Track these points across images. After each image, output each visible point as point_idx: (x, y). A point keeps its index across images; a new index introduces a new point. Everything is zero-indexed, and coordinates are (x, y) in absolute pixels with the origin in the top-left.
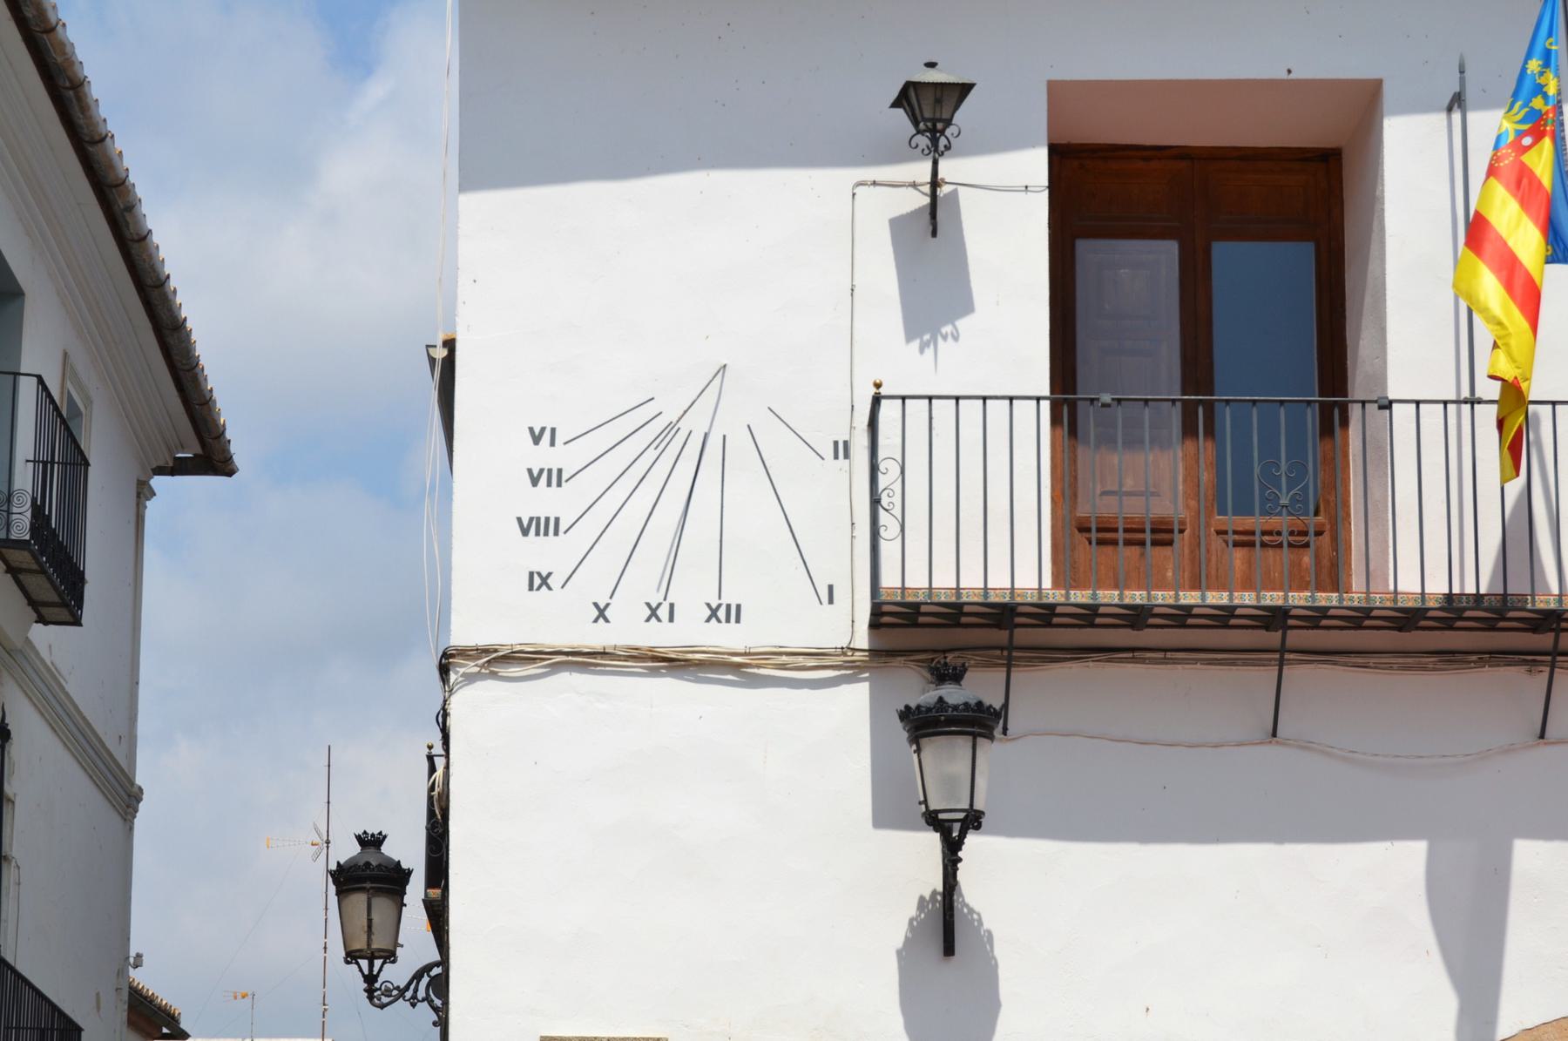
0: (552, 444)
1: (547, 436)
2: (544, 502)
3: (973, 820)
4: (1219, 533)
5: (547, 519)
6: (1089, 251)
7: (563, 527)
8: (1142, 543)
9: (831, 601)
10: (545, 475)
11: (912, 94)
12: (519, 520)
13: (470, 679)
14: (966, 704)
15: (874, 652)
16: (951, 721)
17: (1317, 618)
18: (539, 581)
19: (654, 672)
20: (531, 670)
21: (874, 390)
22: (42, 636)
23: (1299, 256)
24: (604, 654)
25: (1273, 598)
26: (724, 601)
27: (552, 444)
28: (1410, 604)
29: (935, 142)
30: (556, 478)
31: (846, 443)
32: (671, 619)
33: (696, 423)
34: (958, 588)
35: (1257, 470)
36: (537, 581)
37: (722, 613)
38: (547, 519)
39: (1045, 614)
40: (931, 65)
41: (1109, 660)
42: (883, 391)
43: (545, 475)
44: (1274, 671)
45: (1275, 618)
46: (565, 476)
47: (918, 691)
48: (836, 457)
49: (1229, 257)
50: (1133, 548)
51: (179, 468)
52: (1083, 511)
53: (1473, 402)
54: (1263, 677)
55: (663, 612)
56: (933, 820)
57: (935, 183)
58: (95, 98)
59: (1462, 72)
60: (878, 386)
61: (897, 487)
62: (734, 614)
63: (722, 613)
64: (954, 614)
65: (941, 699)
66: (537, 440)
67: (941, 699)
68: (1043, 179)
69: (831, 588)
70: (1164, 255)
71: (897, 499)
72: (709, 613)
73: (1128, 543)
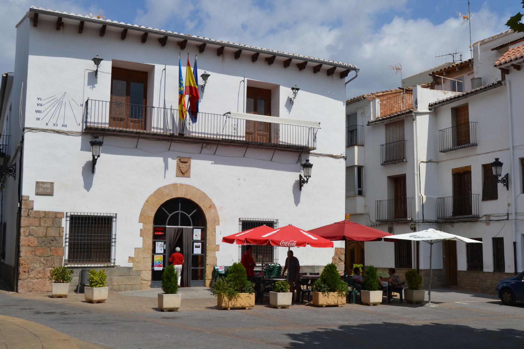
0: (41, 100)
1: (40, 99)
2: (39, 108)
5: (40, 111)
7: (42, 112)
9: (79, 125)
10: (39, 105)
11: (95, 59)
12: (36, 110)
14: (99, 142)
16: (97, 144)
17: (143, 133)
18: (38, 119)
20: (38, 131)
21: (88, 99)
23: (142, 85)
24: (47, 130)
25: (138, 131)
26: (64, 124)
27: (41, 100)
28: (155, 133)
29: (97, 66)
30: (41, 105)
31: (82, 105)
32: (57, 126)
34: (195, 136)
35: (137, 114)
36: (38, 119)
37: (64, 126)
38: (40, 111)
39: (109, 130)
40: (97, 56)
41: (153, 140)
42: (89, 99)
43: (39, 105)
44: (137, 139)
46: (42, 105)
48: (81, 106)
49: (133, 84)
52: (112, 116)
54: (273, 151)
55: (56, 125)
58: (495, 160)
60: (88, 98)
61: (232, 130)
62: (66, 126)
63: (64, 126)
65: (96, 141)
66: (38, 99)
67: (96, 141)
68: (111, 72)
69: (79, 124)
71: (90, 113)
72: (62, 125)
73: (117, 120)
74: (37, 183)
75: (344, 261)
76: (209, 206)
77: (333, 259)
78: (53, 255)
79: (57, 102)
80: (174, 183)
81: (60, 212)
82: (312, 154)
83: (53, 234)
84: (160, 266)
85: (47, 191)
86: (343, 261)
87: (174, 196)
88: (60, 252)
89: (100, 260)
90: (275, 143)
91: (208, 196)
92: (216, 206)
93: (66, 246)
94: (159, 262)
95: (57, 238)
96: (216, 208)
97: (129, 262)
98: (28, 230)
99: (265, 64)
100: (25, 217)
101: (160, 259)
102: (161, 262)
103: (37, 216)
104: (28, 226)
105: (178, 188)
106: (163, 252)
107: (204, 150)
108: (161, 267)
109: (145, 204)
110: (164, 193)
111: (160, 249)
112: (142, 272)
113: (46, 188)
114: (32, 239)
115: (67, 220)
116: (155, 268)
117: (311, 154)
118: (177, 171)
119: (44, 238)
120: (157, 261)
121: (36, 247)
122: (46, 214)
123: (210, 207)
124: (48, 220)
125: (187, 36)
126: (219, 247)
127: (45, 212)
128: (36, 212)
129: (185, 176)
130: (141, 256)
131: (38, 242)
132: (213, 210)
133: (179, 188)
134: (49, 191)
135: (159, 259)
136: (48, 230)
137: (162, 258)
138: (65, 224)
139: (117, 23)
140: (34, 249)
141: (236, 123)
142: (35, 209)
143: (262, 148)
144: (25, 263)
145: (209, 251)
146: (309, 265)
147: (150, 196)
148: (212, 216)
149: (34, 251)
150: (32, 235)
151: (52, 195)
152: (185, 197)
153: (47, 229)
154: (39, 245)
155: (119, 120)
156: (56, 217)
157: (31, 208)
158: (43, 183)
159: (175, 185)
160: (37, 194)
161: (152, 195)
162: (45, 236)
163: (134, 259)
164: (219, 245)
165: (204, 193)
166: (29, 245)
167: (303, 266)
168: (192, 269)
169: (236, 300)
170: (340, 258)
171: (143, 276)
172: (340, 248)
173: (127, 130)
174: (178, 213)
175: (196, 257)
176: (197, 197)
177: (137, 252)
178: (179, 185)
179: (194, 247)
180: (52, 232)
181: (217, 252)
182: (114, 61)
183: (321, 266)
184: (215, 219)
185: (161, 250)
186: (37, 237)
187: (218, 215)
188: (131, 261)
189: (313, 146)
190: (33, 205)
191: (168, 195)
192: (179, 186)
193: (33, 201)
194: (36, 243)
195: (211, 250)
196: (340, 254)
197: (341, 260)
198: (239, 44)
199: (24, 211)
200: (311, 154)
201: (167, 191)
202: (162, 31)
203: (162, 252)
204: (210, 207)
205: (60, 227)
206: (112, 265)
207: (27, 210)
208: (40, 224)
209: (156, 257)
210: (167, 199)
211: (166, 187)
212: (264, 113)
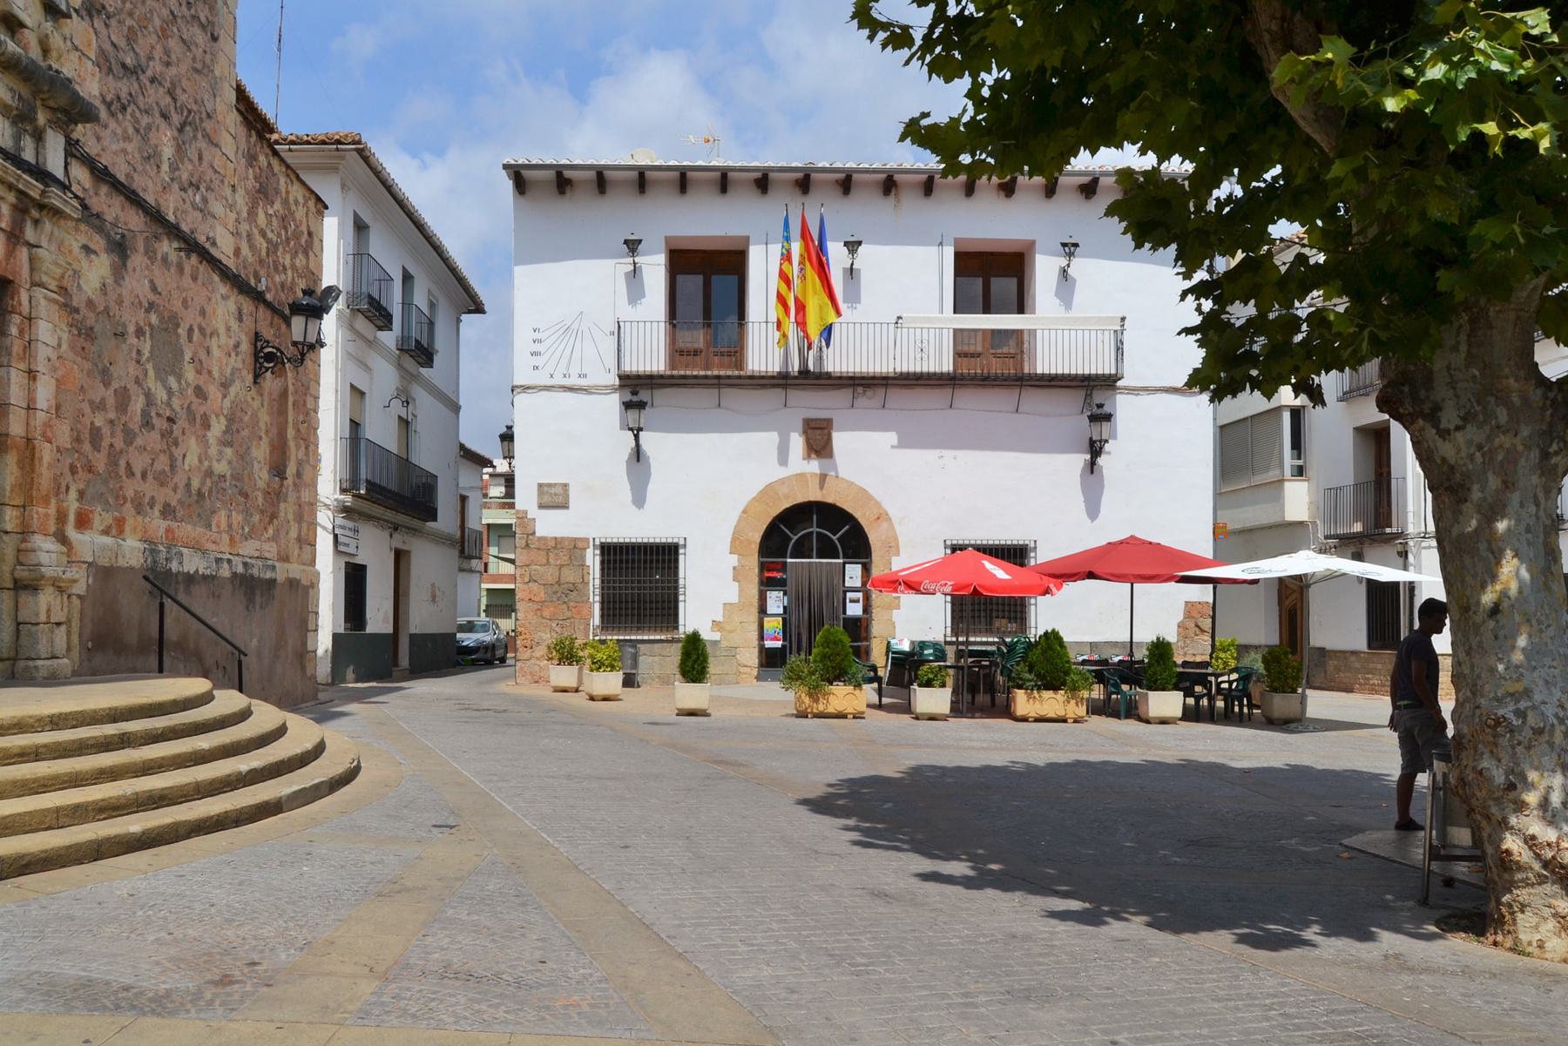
3: (640, 429)
6: (680, 278)
15: (620, 386)
17: (740, 377)
22: (423, 371)
30: (540, 341)
33: (575, 326)
39: (662, 377)
45: (718, 377)
47: (628, 397)
50: (147, 583)
51: (470, 312)
56: (631, 429)
57: (635, 263)
62: (585, 376)
64: (638, 377)
70: (699, 279)
74: (540, 486)
77: (1179, 627)
83: (571, 579)
84: (776, 639)
87: (800, 499)
88: (585, 612)
96: (890, 520)
109: (740, 517)
113: (556, 494)
119: (557, 586)
122: (558, 542)
132: (885, 525)
134: (560, 500)
135: (773, 625)
138: (593, 560)
142: (537, 534)
143: (994, 386)
150: (535, 581)
151: (567, 508)
156: (575, 547)
158: (550, 485)
160: (541, 506)
174: (812, 532)
180: (569, 576)
185: (779, 607)
191: (787, 497)
194: (542, 595)
197: (1203, 631)
199: (520, 539)
201: (784, 490)
203: (781, 611)
205: (583, 565)
209: (769, 622)
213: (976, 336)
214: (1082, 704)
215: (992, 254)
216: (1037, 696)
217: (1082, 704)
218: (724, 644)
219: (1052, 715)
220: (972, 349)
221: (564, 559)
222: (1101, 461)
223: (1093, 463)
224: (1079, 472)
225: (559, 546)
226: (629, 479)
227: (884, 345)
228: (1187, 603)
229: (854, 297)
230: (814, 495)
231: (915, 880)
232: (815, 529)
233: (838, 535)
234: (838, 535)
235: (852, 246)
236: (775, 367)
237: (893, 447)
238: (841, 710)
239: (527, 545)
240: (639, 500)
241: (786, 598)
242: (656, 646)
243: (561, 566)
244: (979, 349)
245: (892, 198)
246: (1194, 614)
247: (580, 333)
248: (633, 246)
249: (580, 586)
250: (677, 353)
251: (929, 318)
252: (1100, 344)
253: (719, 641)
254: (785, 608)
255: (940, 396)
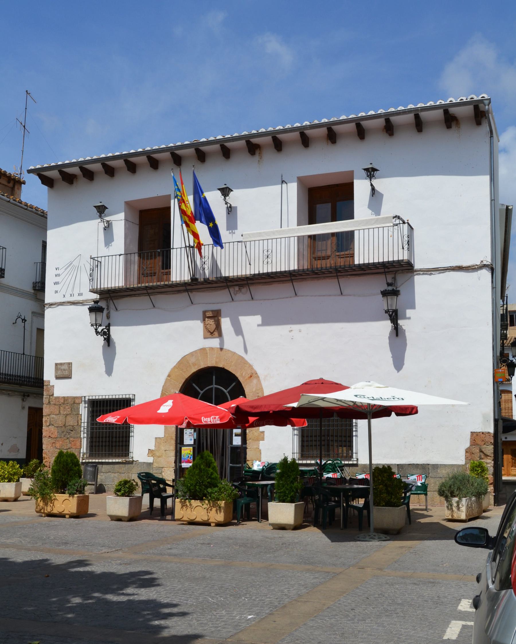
4: (162, 273)
8: (152, 276)
13: (47, 308)
18: (56, 292)
19: (71, 305)
24: (64, 303)
41: (173, 294)
53: (400, 224)
55: (72, 295)
59: (282, 177)
74: (56, 364)
75: (492, 455)
76: (249, 376)
77: (466, 452)
78: (71, 448)
79: (71, 270)
80: (202, 348)
81: (79, 397)
82: (418, 271)
83: (71, 423)
84: (188, 462)
85: (65, 374)
86: (491, 457)
87: (202, 366)
88: (78, 444)
89: (99, 454)
90: (177, 280)
91: (247, 361)
92: (259, 374)
93: (84, 437)
94: (188, 457)
95: (76, 427)
96: (259, 377)
97: (148, 456)
98: (49, 420)
99: (328, 142)
100: (46, 404)
101: (189, 452)
102: (190, 456)
103: (57, 403)
104: (49, 415)
105: (207, 353)
106: (193, 443)
107: (237, 297)
108: (190, 463)
109: (167, 380)
110: (190, 362)
111: (189, 439)
112: (163, 469)
113: (64, 370)
114: (52, 429)
115: (85, 407)
116: (182, 464)
117: (416, 271)
118: (204, 331)
119: (64, 428)
120: (185, 455)
121: (56, 438)
122: (65, 399)
123: (251, 376)
124: (67, 407)
125: (194, 142)
126: (264, 435)
127: (64, 397)
128: (58, 398)
129: (214, 336)
130: (163, 448)
131: (58, 432)
132: (255, 381)
133: (208, 354)
134: (66, 373)
135: (187, 452)
136: (67, 418)
137: (192, 451)
138: (84, 411)
139: (404, 109)
140: (54, 441)
141: (270, 247)
142: (55, 395)
143: (325, 278)
144: (47, 457)
145: (250, 441)
146: (418, 463)
147: (173, 368)
148: (254, 390)
149: (54, 443)
150: (53, 425)
151: (70, 378)
152: (217, 366)
153: (66, 417)
154: (59, 436)
155: (320, 260)
156: (74, 403)
157: (51, 394)
158: (61, 364)
159: (203, 350)
160: (57, 378)
161: (175, 366)
162: (64, 425)
163: (154, 452)
164: (264, 432)
165: (242, 357)
166: (50, 437)
167: (406, 464)
168: (231, 467)
169: (53, 505)
170: (483, 450)
171: (165, 475)
172: (483, 433)
173: (166, 284)
174: (212, 388)
175: (235, 449)
176: (232, 364)
177: (158, 443)
178: (209, 350)
179: (234, 435)
180: (71, 421)
181: (261, 442)
182: (301, 181)
183: (440, 465)
184: (258, 393)
185: (191, 440)
186: (57, 427)
187: (262, 388)
188: (150, 455)
189: (96, 288)
190: (53, 390)
191: (194, 364)
192: (208, 351)
193: (53, 386)
194: (56, 433)
195: (253, 440)
196: (483, 443)
197: (487, 456)
198: (266, 130)
199: (46, 398)
200: (416, 271)
201: (193, 360)
202: (323, 121)
203: (192, 442)
204: (251, 376)
205: (78, 415)
206: (355, 462)
207: (48, 396)
208: (60, 412)
209: (185, 450)
210: (194, 370)
211: (192, 354)
212: (330, 221)
213: (181, 250)
214: (220, 512)
215: (337, 185)
216: (188, 504)
217: (220, 512)
218: (155, 465)
219: (198, 519)
220: (323, 254)
221: (68, 411)
222: (209, 333)
223: (397, 331)
224: (388, 335)
225: (66, 402)
226: (104, 358)
227: (257, 255)
228: (472, 433)
229: (232, 226)
230: (211, 362)
231: (204, 633)
232: (214, 386)
233: (228, 390)
234: (228, 390)
235: (225, 192)
236: (187, 277)
237: (259, 325)
238: (61, 511)
239: (49, 402)
240: (109, 371)
241: (195, 434)
242: (117, 466)
243: (67, 415)
244: (329, 253)
245: (257, 157)
246: (479, 442)
247: (79, 267)
248: (101, 210)
249: (76, 428)
250: (143, 274)
251: (260, 233)
252: (391, 239)
253: (152, 464)
254: (195, 440)
255: (286, 289)
